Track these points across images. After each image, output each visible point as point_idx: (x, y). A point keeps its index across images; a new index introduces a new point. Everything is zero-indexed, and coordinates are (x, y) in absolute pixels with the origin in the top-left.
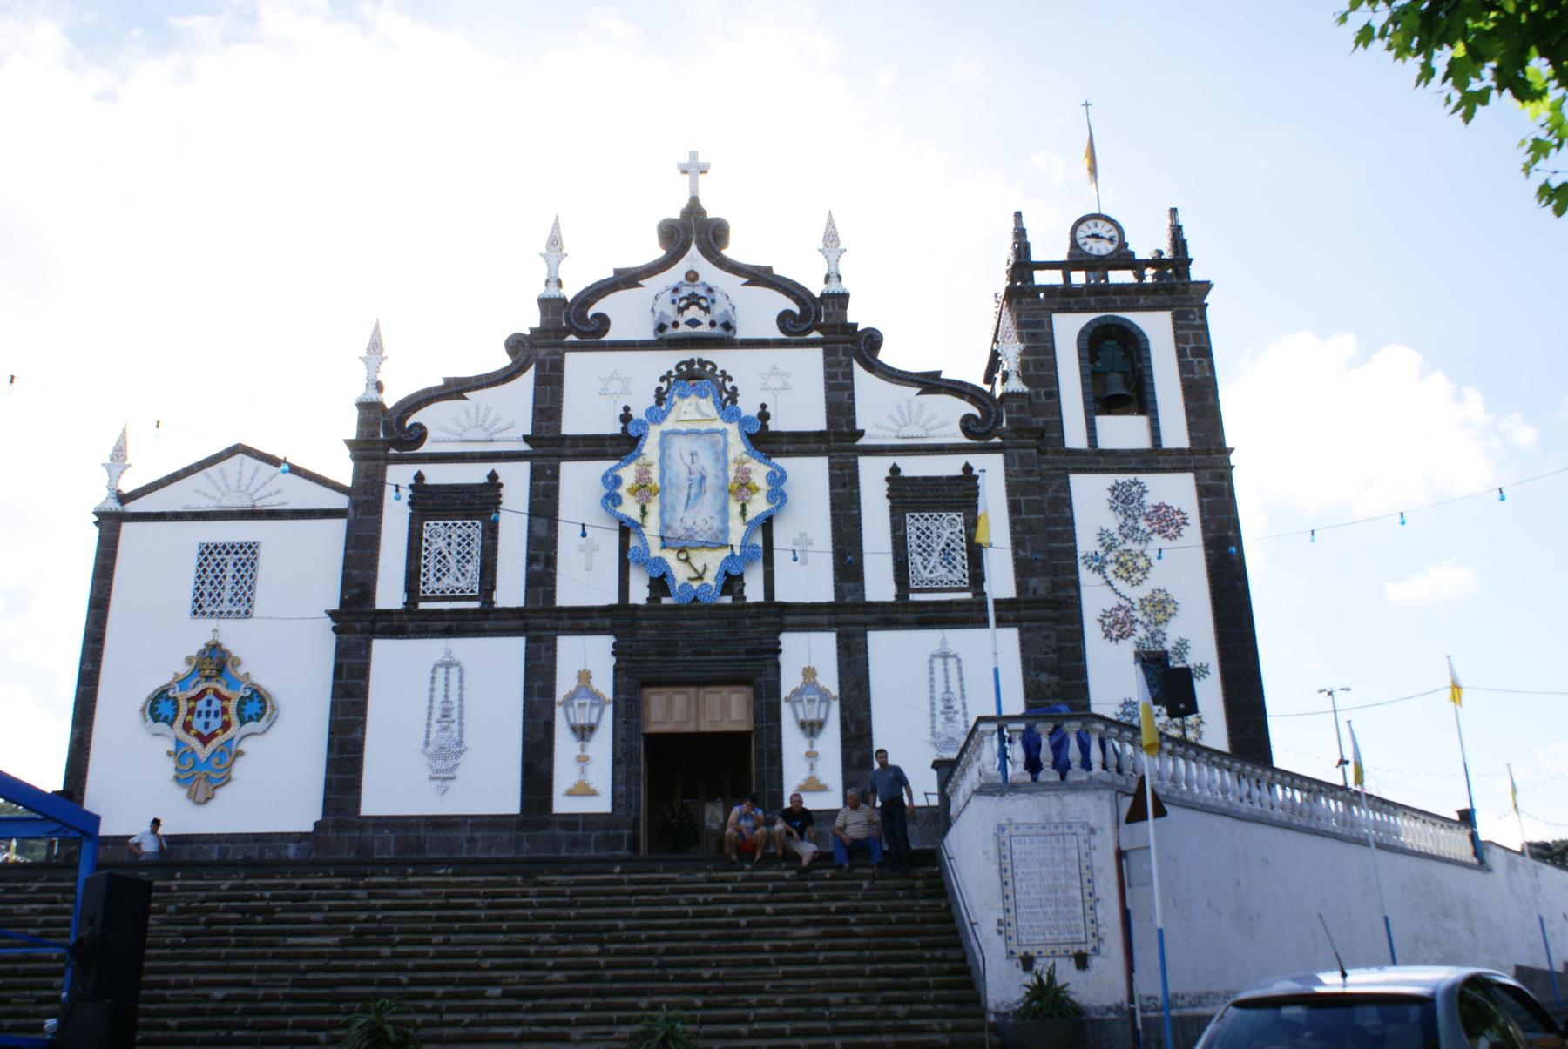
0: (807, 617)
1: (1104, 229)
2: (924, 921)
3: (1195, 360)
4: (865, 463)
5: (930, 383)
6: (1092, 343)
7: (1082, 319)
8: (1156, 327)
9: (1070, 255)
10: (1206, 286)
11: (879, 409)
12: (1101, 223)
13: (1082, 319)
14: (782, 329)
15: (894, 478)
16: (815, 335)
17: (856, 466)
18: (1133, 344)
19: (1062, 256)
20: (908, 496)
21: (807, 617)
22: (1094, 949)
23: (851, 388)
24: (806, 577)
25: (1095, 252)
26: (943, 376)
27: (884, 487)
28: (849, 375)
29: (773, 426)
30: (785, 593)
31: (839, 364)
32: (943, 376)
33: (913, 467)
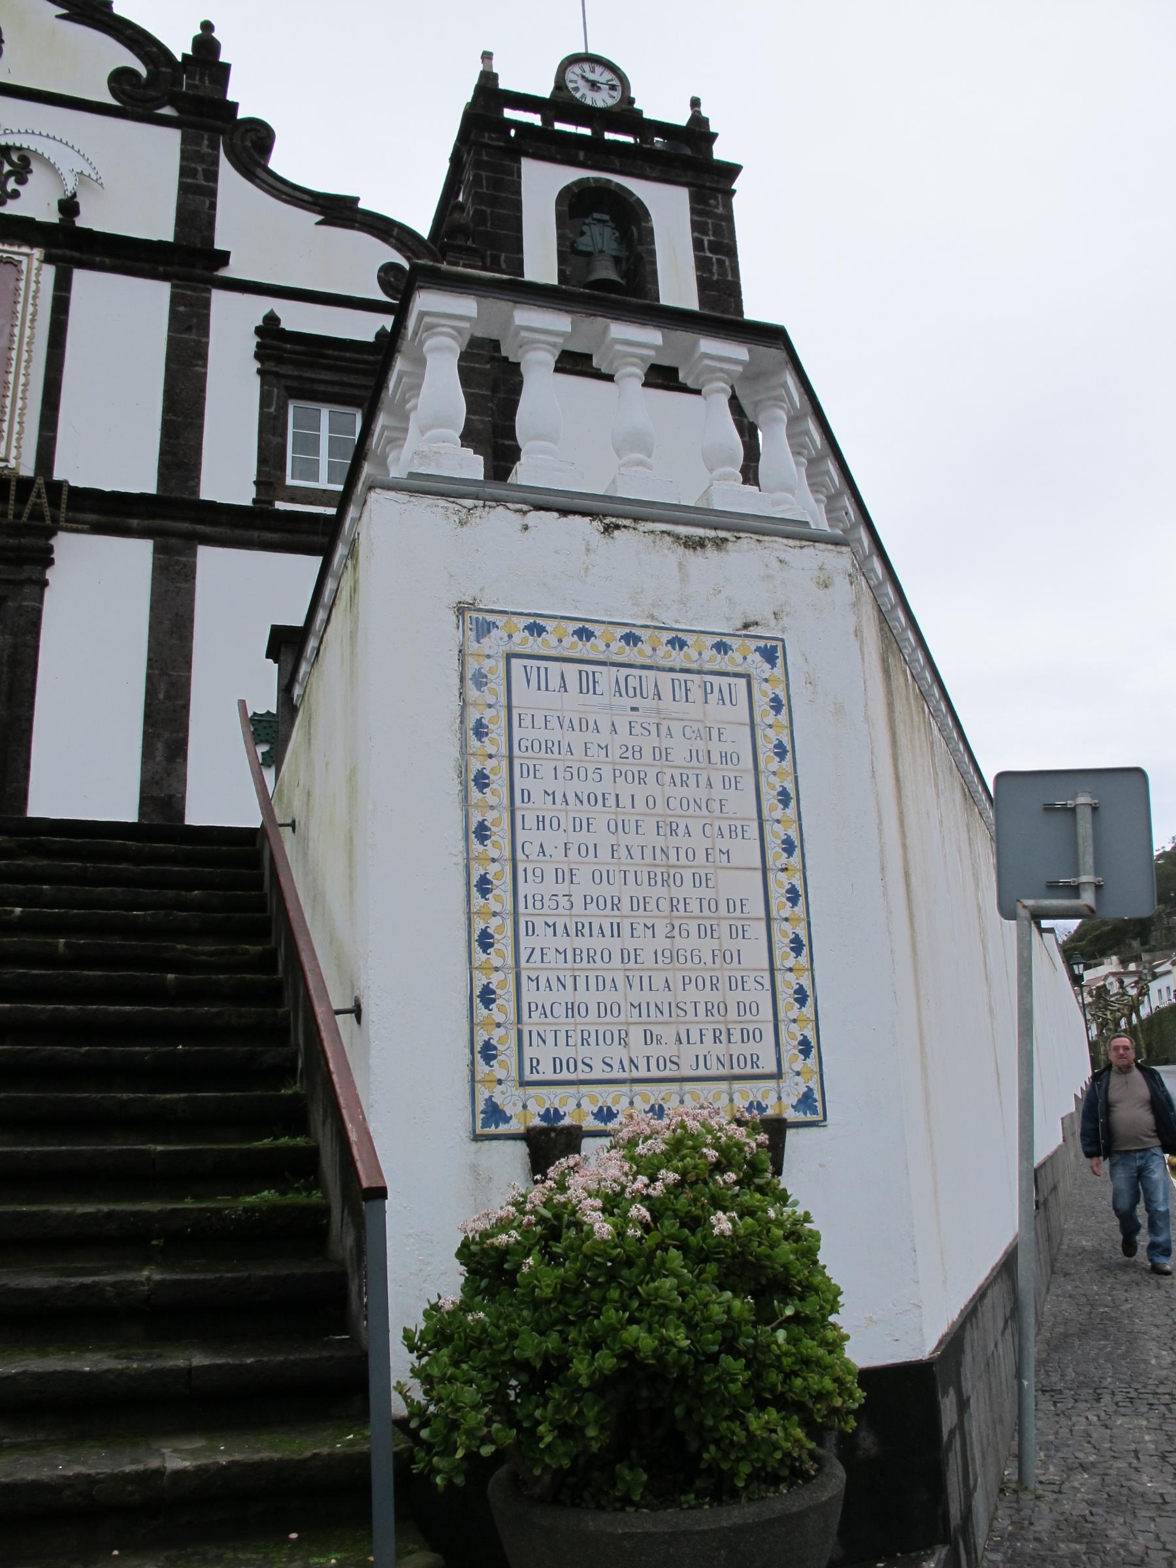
0: (109, 512)
1: (601, 75)
2: (79, 960)
3: (714, 257)
4: (220, 299)
5: (339, 211)
6: (575, 206)
7: (570, 175)
8: (667, 207)
9: (553, 94)
10: (732, 171)
11: (244, 222)
12: (599, 69)
13: (570, 175)
14: (114, 92)
15: (269, 329)
16: (167, 111)
17: (207, 304)
18: (632, 220)
19: (544, 89)
20: (296, 367)
21: (109, 512)
22: (806, 1102)
23: (213, 193)
24: (110, 447)
25: (589, 102)
26: (361, 205)
27: (251, 342)
28: (212, 176)
29: (81, 222)
30: (71, 469)
31: (202, 158)
32: (361, 205)
33: (298, 319)
